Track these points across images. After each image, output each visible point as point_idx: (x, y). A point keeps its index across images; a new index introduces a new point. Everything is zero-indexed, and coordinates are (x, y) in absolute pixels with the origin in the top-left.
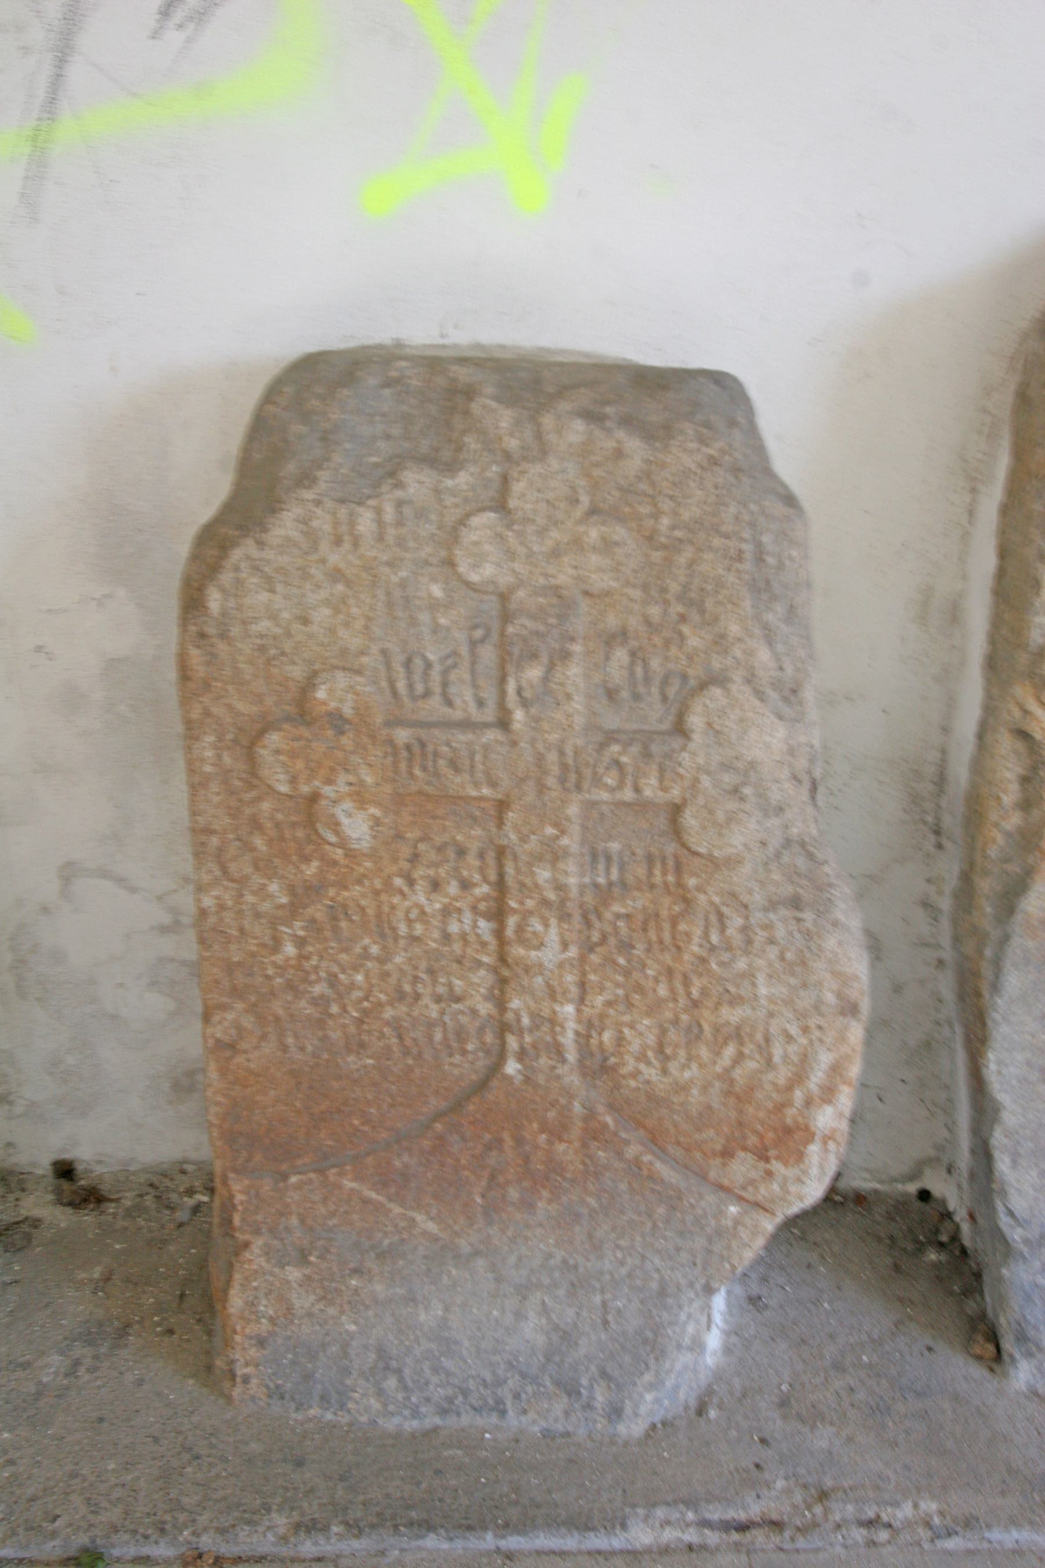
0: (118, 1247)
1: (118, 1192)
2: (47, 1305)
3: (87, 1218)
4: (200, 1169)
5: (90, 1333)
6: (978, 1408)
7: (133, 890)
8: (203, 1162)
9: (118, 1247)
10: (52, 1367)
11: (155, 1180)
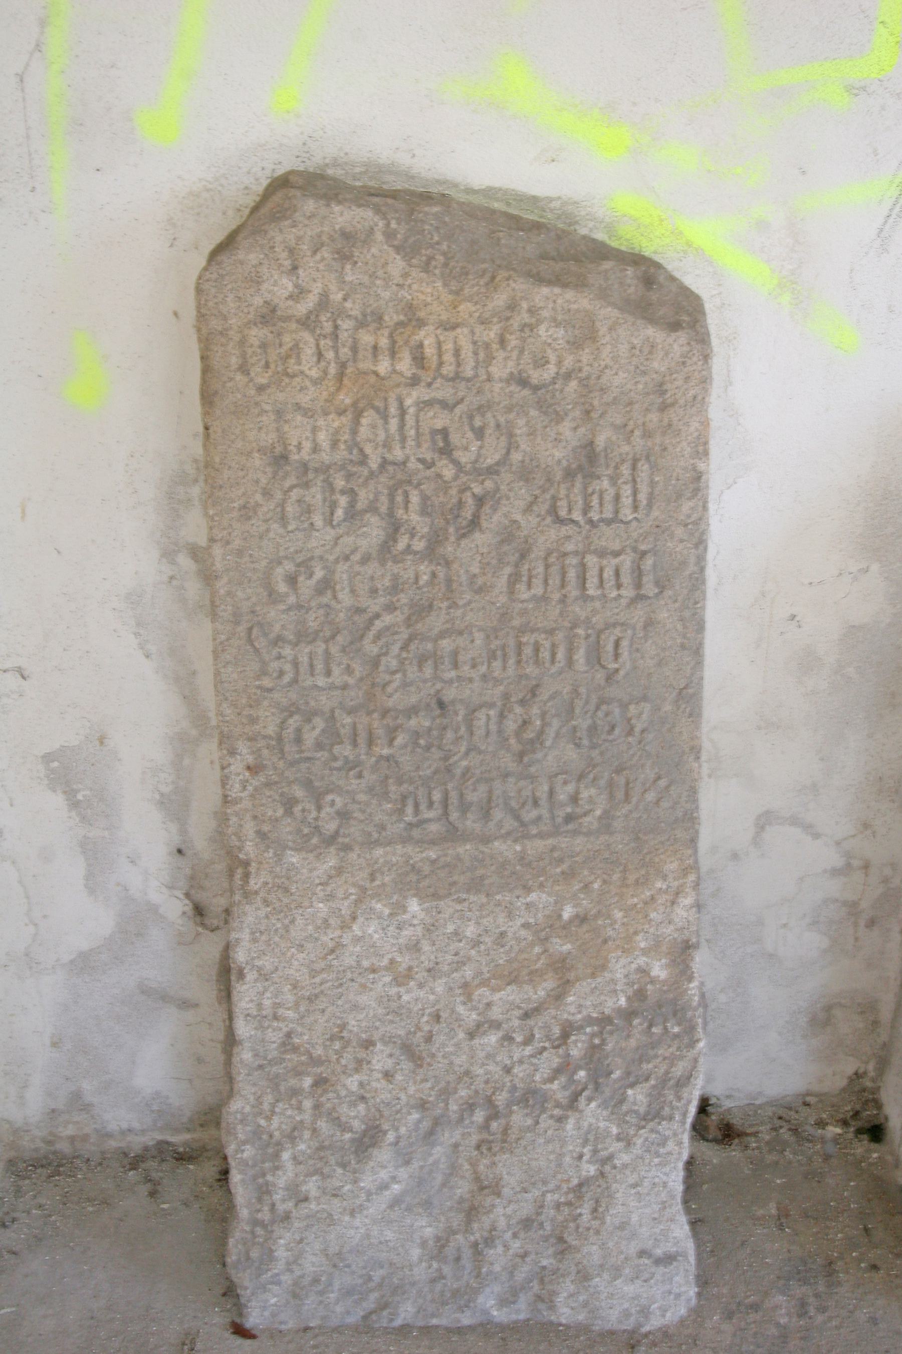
0: (778, 1181)
1: (751, 1126)
2: (743, 1243)
3: (734, 1153)
4: (821, 1101)
5: (799, 1273)
6: (800, 1316)
7: (817, 836)
8: (825, 1094)
9: (778, 1181)
10: (781, 1306)
11: (781, 1112)
